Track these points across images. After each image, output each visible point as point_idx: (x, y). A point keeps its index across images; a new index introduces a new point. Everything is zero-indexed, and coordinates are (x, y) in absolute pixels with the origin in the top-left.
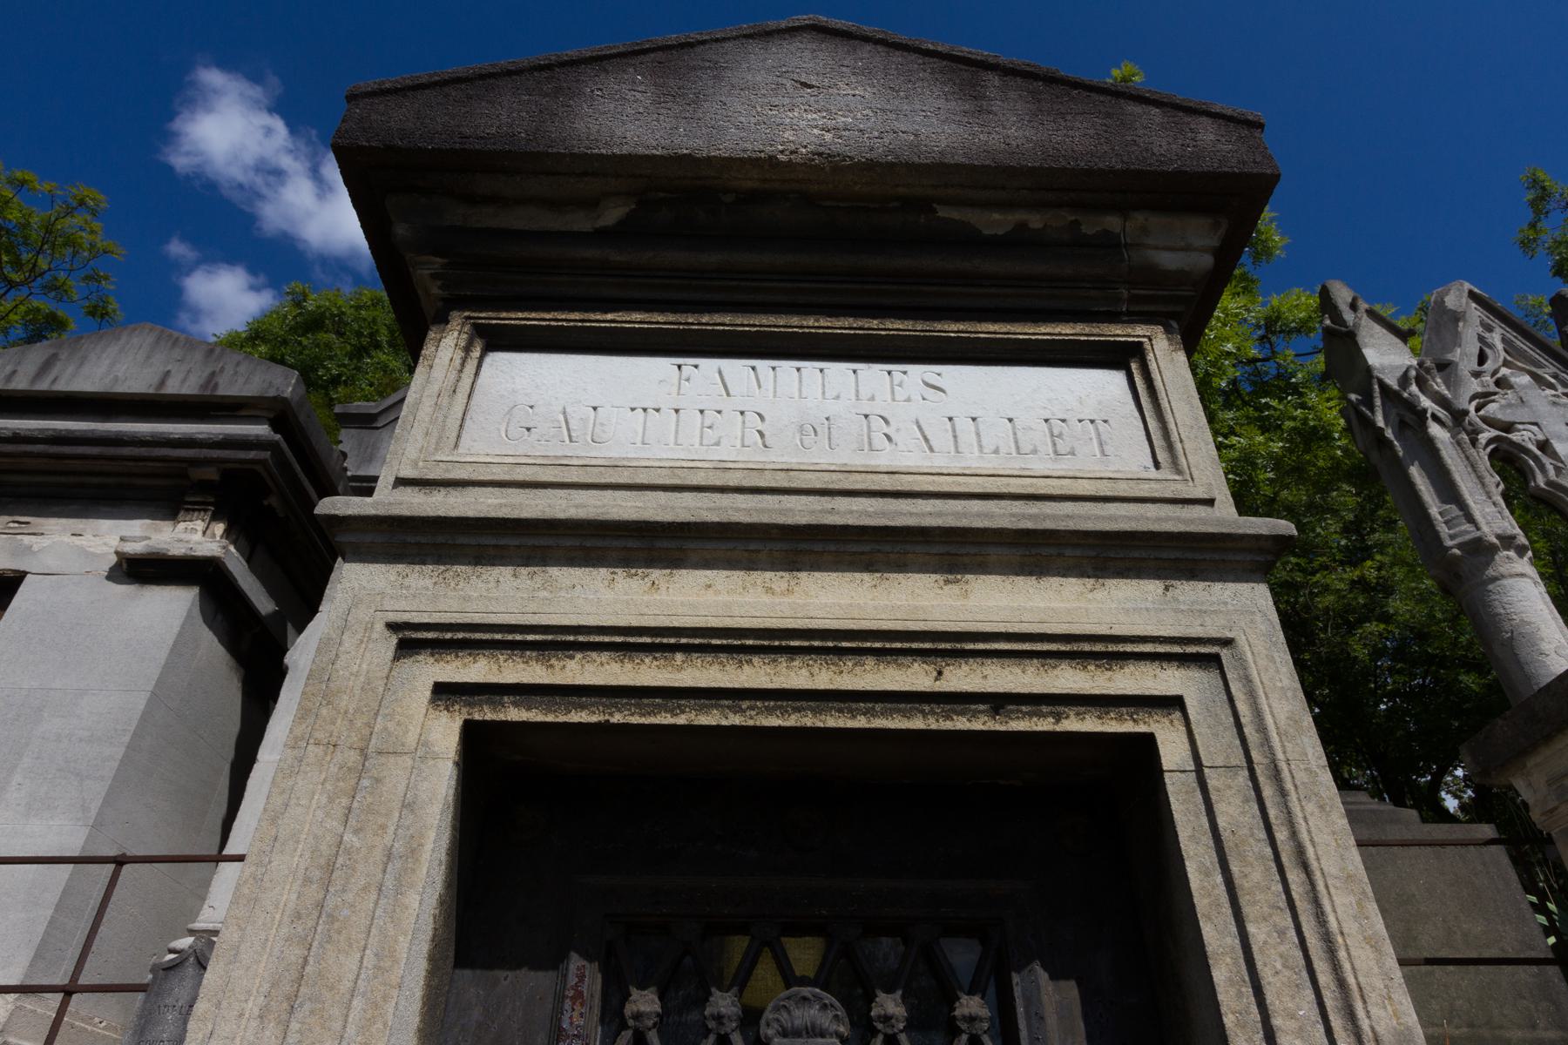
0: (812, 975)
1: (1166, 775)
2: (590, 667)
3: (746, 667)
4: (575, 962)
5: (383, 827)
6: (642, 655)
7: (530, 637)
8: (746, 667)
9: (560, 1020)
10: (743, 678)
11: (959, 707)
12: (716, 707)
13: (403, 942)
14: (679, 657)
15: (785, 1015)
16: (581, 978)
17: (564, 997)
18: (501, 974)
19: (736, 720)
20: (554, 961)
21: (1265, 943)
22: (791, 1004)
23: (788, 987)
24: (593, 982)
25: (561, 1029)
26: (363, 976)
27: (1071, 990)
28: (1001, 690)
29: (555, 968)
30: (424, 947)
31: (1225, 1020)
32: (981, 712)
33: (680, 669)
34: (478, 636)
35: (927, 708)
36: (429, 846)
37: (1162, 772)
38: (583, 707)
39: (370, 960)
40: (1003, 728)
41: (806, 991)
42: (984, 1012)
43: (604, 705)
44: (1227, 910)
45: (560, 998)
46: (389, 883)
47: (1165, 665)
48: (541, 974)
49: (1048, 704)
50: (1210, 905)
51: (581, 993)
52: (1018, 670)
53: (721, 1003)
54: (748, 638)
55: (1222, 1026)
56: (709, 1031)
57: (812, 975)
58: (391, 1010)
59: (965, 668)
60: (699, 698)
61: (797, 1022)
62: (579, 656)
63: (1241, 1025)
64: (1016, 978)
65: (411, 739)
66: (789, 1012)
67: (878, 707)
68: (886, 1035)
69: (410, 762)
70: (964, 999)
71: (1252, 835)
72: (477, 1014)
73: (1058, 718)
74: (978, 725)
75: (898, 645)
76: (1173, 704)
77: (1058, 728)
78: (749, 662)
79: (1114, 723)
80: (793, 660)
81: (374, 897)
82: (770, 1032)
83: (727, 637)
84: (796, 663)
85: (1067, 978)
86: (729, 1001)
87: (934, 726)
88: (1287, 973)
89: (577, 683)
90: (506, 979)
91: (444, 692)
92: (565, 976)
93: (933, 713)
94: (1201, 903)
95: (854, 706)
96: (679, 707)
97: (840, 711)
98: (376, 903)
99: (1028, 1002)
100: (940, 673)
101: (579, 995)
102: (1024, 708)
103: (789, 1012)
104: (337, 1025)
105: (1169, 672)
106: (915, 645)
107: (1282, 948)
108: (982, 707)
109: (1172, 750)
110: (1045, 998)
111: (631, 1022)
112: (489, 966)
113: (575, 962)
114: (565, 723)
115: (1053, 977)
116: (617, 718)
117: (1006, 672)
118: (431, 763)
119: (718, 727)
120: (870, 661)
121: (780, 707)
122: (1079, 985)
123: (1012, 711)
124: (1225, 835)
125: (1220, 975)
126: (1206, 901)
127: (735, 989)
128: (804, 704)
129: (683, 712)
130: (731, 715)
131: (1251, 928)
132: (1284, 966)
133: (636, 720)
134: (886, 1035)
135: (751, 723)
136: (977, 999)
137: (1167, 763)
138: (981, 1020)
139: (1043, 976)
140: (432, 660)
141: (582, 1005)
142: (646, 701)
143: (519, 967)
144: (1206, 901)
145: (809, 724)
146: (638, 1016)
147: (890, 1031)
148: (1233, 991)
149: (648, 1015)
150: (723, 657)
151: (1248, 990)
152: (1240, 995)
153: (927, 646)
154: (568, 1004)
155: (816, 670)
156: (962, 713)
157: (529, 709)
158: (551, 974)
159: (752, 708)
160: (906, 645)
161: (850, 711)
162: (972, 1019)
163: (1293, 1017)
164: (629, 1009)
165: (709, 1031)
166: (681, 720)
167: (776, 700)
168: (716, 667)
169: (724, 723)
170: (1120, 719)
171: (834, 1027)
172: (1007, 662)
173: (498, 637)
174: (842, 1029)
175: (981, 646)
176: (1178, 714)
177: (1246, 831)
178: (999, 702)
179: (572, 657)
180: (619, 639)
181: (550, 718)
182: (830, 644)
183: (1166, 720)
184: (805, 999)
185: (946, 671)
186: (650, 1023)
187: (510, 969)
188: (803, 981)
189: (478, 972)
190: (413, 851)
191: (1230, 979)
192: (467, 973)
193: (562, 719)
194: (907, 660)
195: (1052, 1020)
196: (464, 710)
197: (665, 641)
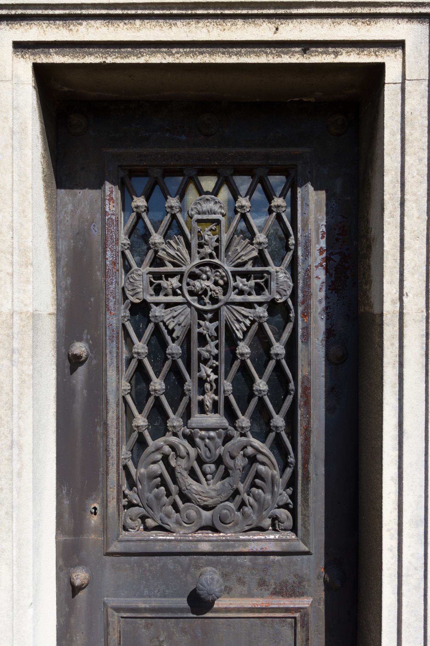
0: (211, 191)
1: (386, 86)
2: (91, 30)
3: (173, 28)
4: (108, 186)
5: (6, 118)
6: (118, 22)
7: (57, 12)
8: (173, 28)
9: (105, 208)
10: (173, 34)
11: (285, 50)
12: (159, 52)
13: (29, 170)
14: (138, 22)
15: (199, 206)
16: (112, 192)
17: (105, 199)
18: (78, 191)
19: (169, 60)
20: (99, 186)
21: (412, 164)
22: (202, 202)
23: (200, 195)
24: (117, 194)
25: (106, 212)
26: (15, 184)
27: (323, 194)
28: (309, 39)
29: (100, 188)
30: (40, 175)
31: (385, 197)
32: (296, 52)
33: (139, 30)
34: (29, 12)
35: (268, 50)
36: (30, 128)
37: (384, 83)
38: (91, 54)
39: (16, 178)
40: (307, 61)
41: (208, 197)
42: (284, 204)
43: (102, 53)
44: (399, 151)
45: (103, 200)
46: (16, 144)
47: (400, 21)
48: (94, 191)
49: (332, 47)
50: (391, 149)
51: (112, 198)
52: (319, 26)
53: (172, 201)
54: (173, 9)
55: (383, 200)
56: (168, 213)
57: (211, 191)
58: (30, 197)
59: (291, 25)
60: (150, 47)
61: (204, 209)
62: (85, 23)
63: (391, 199)
64: (299, 190)
65: (9, 76)
66: (201, 205)
67: (243, 50)
68: (241, 213)
69: (11, 86)
70: (276, 199)
71: (420, 115)
72: (70, 207)
73: (336, 54)
74: (294, 60)
75: (255, 12)
76: (399, 44)
77: (336, 61)
78: (175, 24)
79: (365, 57)
80: (198, 22)
81: (10, 150)
82: (193, 213)
83: (163, 9)
84: (200, 25)
85: (321, 189)
86: (175, 201)
87: (271, 61)
88: (418, 177)
89: (86, 40)
90: (80, 193)
91: (19, 46)
92: (104, 191)
93: (271, 53)
94: (387, 147)
95: (231, 50)
96: (140, 53)
97: (223, 53)
98: (12, 153)
99: (303, 199)
100: (277, 29)
101: (111, 199)
102: (319, 50)
103: (201, 205)
104: (10, 203)
105: (401, 26)
106: (265, 11)
107: (419, 167)
108: (297, 49)
109: (392, 74)
110: (310, 197)
111: (135, 210)
112: (72, 188)
113: (108, 186)
114: (83, 64)
115: (316, 189)
116: (109, 60)
117: (313, 27)
118: (21, 86)
119: (161, 64)
120: (240, 22)
121: (192, 52)
122: (326, 192)
123: (313, 52)
124: (407, 114)
125: (387, 179)
126: (390, 147)
127: (178, 196)
128: (205, 49)
129: (143, 56)
130: (167, 57)
131: (407, 158)
132: (418, 174)
133: (119, 61)
134: (241, 213)
135: (177, 61)
136: (281, 199)
137: (387, 79)
138: (282, 207)
139: (310, 188)
140: (8, 28)
141: (113, 202)
142: (123, 50)
143: (84, 188)
144: (390, 147)
145: (207, 61)
146: (137, 207)
147: (243, 212)
148: (391, 186)
149: (142, 207)
150: (161, 21)
151: (399, 185)
152: (394, 187)
153: (272, 11)
154: (107, 202)
155: (210, 28)
156: (286, 53)
157: (64, 56)
158: (98, 191)
159: (177, 53)
160: (260, 12)
161: (229, 53)
162: (278, 207)
163: (415, 195)
164: (133, 204)
165: (168, 213)
166: (142, 60)
167: (190, 48)
168: (158, 28)
169: (164, 61)
170: (369, 54)
171: (220, 210)
172: (314, 21)
173: (40, 12)
174: (223, 211)
175: (301, 11)
176: (400, 51)
177: (418, 113)
178: (306, 46)
179: (81, 24)
180: (104, 12)
181: (75, 61)
182: (219, 12)
183: (393, 55)
184: (208, 200)
185: (280, 28)
186: (143, 210)
187: (81, 189)
188: (207, 193)
189: (68, 190)
190: (23, 130)
191: (392, 181)
192: (63, 191)
193: (81, 61)
194: (259, 21)
195: (312, 206)
196: (32, 57)
197: (129, 12)
